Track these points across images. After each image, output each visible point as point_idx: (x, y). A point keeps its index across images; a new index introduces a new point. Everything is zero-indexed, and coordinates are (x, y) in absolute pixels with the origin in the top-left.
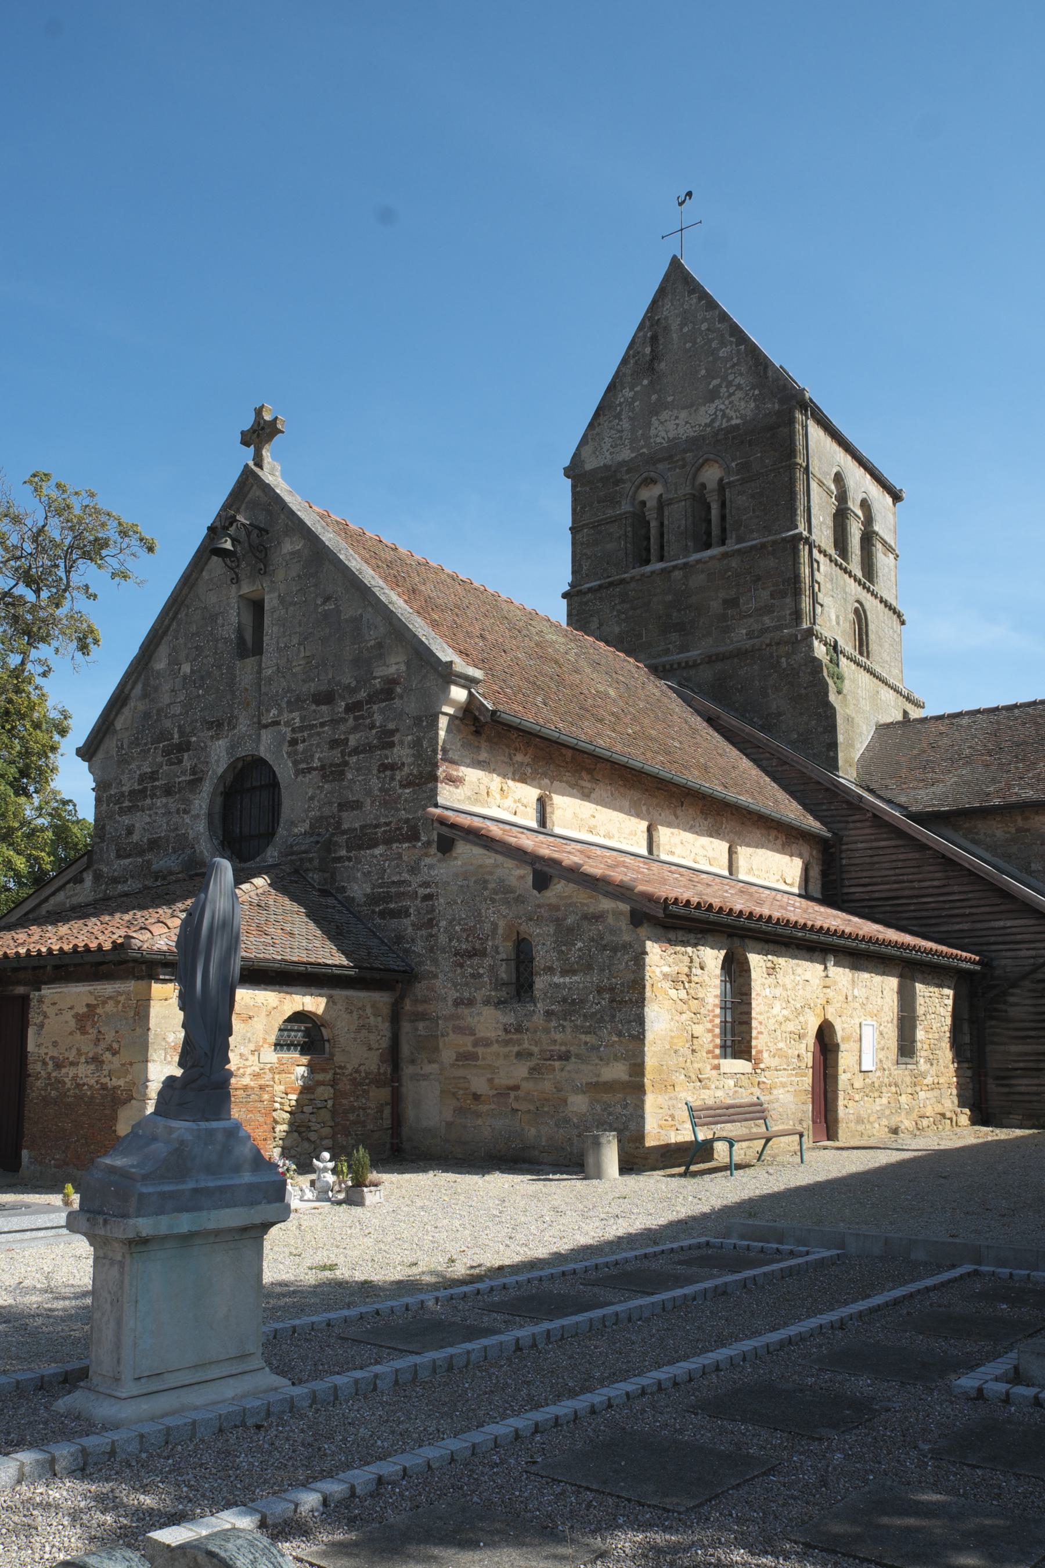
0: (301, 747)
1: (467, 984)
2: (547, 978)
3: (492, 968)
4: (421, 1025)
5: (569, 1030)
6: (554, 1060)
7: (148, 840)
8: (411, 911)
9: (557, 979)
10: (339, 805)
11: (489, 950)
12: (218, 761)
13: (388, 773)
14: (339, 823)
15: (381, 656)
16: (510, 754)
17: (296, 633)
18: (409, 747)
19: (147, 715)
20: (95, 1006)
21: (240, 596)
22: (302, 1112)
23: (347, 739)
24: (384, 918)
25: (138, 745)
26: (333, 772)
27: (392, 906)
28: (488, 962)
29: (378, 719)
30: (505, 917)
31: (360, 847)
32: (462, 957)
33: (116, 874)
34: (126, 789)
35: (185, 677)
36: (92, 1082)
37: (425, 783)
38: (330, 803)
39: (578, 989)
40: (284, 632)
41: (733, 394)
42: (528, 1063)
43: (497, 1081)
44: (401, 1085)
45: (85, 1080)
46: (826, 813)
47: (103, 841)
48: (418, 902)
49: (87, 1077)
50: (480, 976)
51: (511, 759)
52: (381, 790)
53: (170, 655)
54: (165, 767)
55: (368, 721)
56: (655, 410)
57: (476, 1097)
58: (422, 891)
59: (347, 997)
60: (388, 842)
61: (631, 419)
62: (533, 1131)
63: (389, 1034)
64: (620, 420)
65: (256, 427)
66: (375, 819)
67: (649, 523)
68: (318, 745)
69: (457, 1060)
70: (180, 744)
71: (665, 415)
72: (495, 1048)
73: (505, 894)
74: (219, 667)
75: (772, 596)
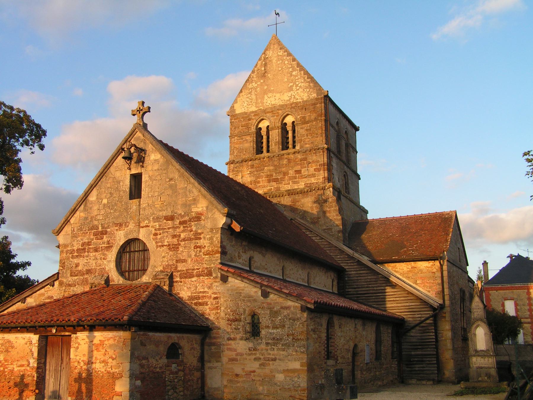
0: (159, 237)
1: (233, 332)
2: (266, 330)
3: (243, 326)
4: (213, 348)
5: (276, 350)
6: (270, 361)
7: (86, 270)
8: (209, 303)
9: (270, 331)
10: (176, 260)
11: (242, 319)
12: (120, 240)
13: (198, 249)
14: (176, 267)
16: (241, 242)
17: (156, 191)
18: (208, 240)
19: (86, 218)
20: (104, 341)
21: (131, 174)
22: (174, 382)
23: (180, 235)
24: (197, 306)
26: (174, 248)
27: (200, 301)
28: (242, 323)
29: (194, 229)
30: (249, 307)
31: (186, 278)
32: (231, 321)
33: (70, 283)
34: (75, 248)
35: (104, 205)
36: (103, 370)
37: (215, 254)
38: (173, 260)
39: (279, 334)
40: (151, 190)
41: (298, 90)
42: (259, 362)
43: (246, 369)
44: (204, 371)
45: (99, 370)
46: (339, 259)
47: (64, 269)
48: (212, 300)
49: (100, 368)
50: (239, 329)
51: (242, 244)
52: (195, 255)
53: (97, 195)
54: (94, 240)
55: (189, 229)
56: (265, 92)
57: (237, 375)
58: (213, 296)
59: (188, 337)
60: (198, 276)
61: (256, 95)
62: (261, 388)
63: (200, 351)
65: (138, 109)
66: (193, 267)
67: (262, 136)
68: (167, 236)
69: (228, 361)
70: (102, 231)
71: (270, 95)
72: (245, 356)
73: (249, 298)
74: (121, 202)
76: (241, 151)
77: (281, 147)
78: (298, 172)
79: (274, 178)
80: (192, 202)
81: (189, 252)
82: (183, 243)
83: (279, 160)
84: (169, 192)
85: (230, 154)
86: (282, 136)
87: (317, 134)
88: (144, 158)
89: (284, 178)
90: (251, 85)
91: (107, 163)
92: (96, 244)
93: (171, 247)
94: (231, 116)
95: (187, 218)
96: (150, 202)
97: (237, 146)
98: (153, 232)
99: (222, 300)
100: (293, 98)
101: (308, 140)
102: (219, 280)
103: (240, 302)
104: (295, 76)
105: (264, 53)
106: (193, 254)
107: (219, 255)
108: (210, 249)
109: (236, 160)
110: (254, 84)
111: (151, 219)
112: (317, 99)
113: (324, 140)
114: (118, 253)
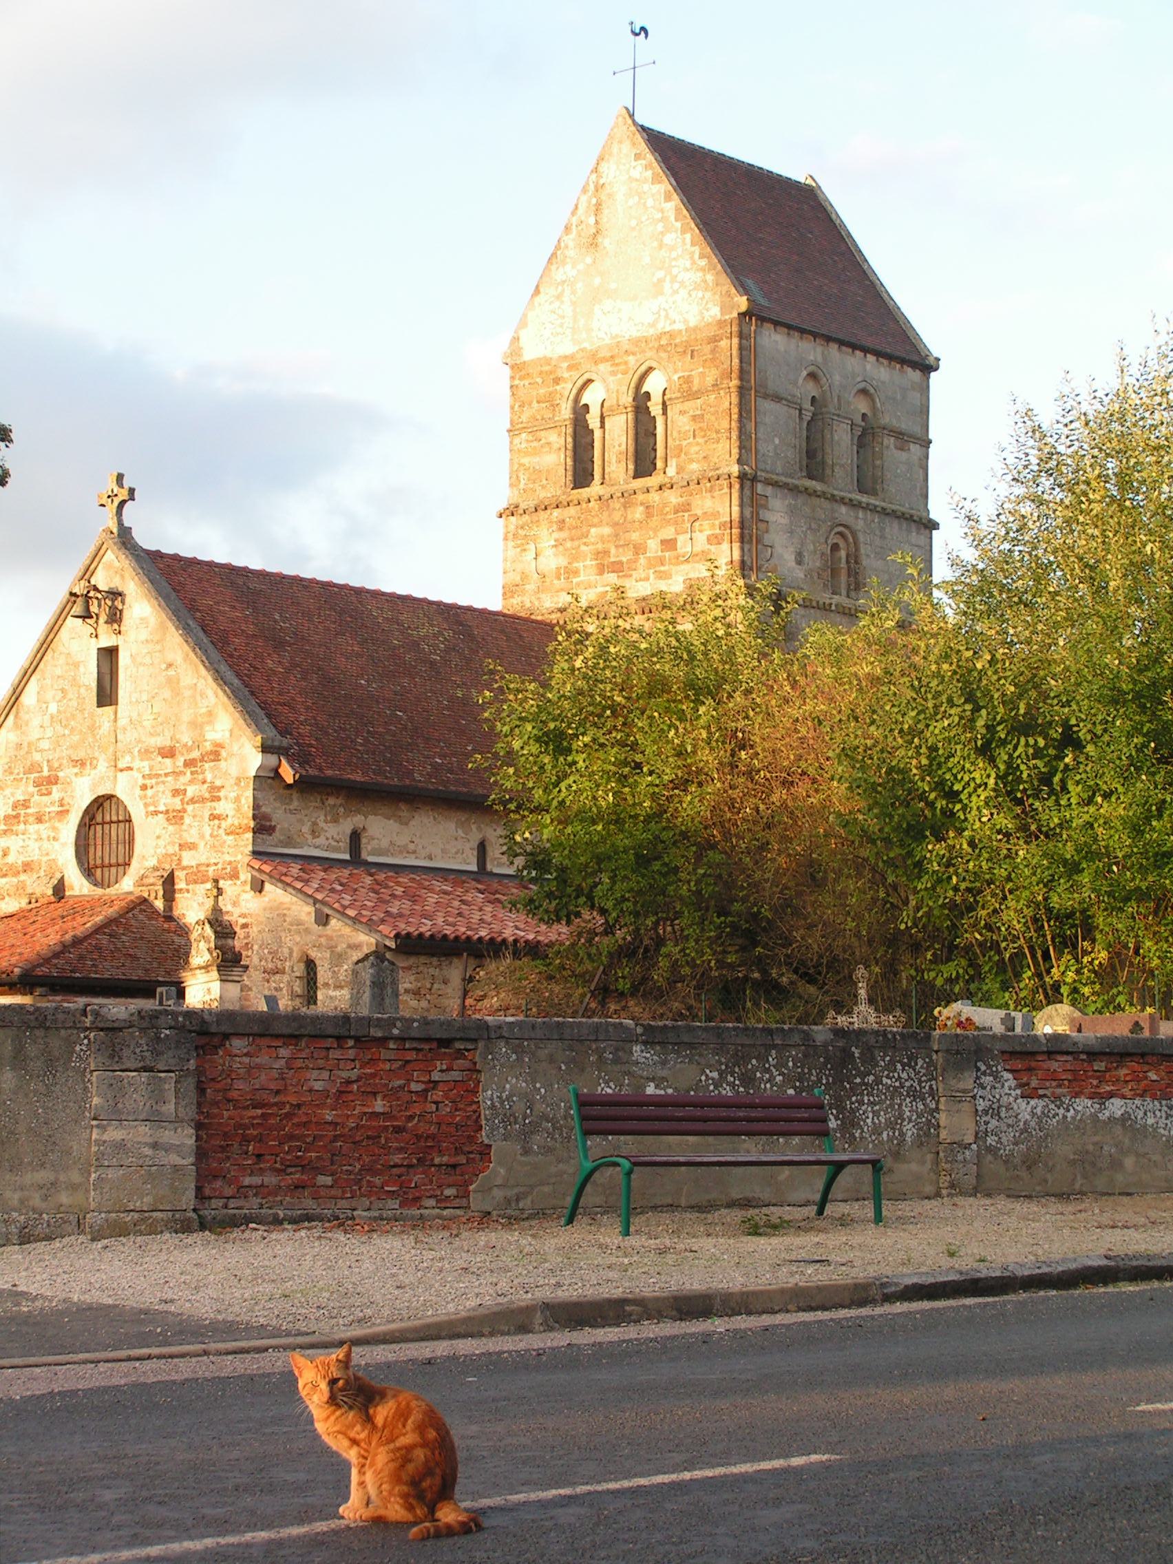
0: (149, 792)
9: (332, 993)
13: (216, 822)
15: (210, 722)
25: (11, 773)
26: (175, 817)
28: (286, 978)
29: (209, 776)
31: (196, 882)
50: (281, 989)
52: (211, 835)
55: (200, 777)
61: (573, 303)
64: (562, 302)
67: (592, 431)
74: (82, 711)
75: (709, 540)
76: (536, 474)
77: (631, 467)
78: (669, 544)
79: (612, 559)
80: (206, 719)
81: (201, 827)
82: (190, 808)
83: (625, 507)
84: (167, 694)
85: (511, 485)
86: (637, 434)
87: (718, 432)
88: (121, 611)
89: (636, 561)
90: (561, 269)
91: (53, 621)
92: (39, 804)
93: (171, 815)
94: (512, 368)
95: (195, 754)
96: (134, 715)
97: (525, 461)
98: (141, 781)
99: (255, 929)
100: (662, 318)
101: (696, 448)
102: (248, 887)
103: (283, 935)
104: (672, 248)
105: (595, 170)
106: (207, 831)
107: (250, 835)
108: (236, 823)
109: (523, 506)
110: (568, 267)
111: (136, 753)
112: (721, 323)
113: (735, 451)
114: (80, 826)
